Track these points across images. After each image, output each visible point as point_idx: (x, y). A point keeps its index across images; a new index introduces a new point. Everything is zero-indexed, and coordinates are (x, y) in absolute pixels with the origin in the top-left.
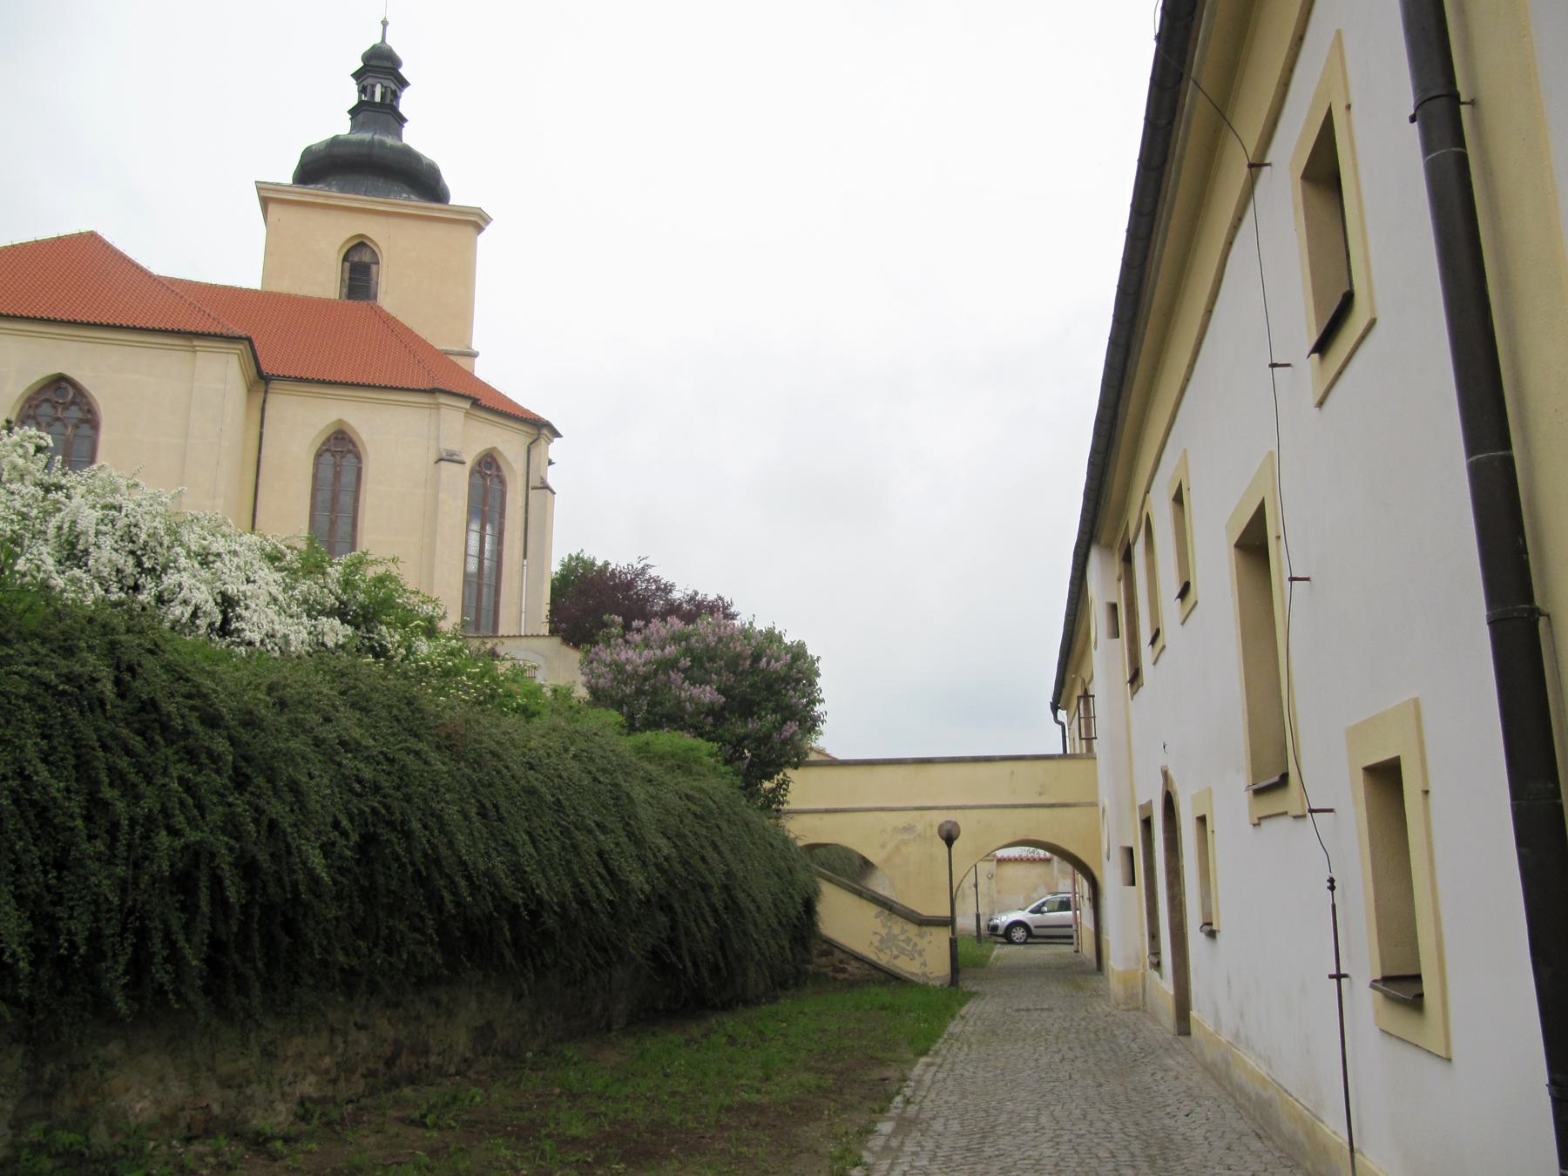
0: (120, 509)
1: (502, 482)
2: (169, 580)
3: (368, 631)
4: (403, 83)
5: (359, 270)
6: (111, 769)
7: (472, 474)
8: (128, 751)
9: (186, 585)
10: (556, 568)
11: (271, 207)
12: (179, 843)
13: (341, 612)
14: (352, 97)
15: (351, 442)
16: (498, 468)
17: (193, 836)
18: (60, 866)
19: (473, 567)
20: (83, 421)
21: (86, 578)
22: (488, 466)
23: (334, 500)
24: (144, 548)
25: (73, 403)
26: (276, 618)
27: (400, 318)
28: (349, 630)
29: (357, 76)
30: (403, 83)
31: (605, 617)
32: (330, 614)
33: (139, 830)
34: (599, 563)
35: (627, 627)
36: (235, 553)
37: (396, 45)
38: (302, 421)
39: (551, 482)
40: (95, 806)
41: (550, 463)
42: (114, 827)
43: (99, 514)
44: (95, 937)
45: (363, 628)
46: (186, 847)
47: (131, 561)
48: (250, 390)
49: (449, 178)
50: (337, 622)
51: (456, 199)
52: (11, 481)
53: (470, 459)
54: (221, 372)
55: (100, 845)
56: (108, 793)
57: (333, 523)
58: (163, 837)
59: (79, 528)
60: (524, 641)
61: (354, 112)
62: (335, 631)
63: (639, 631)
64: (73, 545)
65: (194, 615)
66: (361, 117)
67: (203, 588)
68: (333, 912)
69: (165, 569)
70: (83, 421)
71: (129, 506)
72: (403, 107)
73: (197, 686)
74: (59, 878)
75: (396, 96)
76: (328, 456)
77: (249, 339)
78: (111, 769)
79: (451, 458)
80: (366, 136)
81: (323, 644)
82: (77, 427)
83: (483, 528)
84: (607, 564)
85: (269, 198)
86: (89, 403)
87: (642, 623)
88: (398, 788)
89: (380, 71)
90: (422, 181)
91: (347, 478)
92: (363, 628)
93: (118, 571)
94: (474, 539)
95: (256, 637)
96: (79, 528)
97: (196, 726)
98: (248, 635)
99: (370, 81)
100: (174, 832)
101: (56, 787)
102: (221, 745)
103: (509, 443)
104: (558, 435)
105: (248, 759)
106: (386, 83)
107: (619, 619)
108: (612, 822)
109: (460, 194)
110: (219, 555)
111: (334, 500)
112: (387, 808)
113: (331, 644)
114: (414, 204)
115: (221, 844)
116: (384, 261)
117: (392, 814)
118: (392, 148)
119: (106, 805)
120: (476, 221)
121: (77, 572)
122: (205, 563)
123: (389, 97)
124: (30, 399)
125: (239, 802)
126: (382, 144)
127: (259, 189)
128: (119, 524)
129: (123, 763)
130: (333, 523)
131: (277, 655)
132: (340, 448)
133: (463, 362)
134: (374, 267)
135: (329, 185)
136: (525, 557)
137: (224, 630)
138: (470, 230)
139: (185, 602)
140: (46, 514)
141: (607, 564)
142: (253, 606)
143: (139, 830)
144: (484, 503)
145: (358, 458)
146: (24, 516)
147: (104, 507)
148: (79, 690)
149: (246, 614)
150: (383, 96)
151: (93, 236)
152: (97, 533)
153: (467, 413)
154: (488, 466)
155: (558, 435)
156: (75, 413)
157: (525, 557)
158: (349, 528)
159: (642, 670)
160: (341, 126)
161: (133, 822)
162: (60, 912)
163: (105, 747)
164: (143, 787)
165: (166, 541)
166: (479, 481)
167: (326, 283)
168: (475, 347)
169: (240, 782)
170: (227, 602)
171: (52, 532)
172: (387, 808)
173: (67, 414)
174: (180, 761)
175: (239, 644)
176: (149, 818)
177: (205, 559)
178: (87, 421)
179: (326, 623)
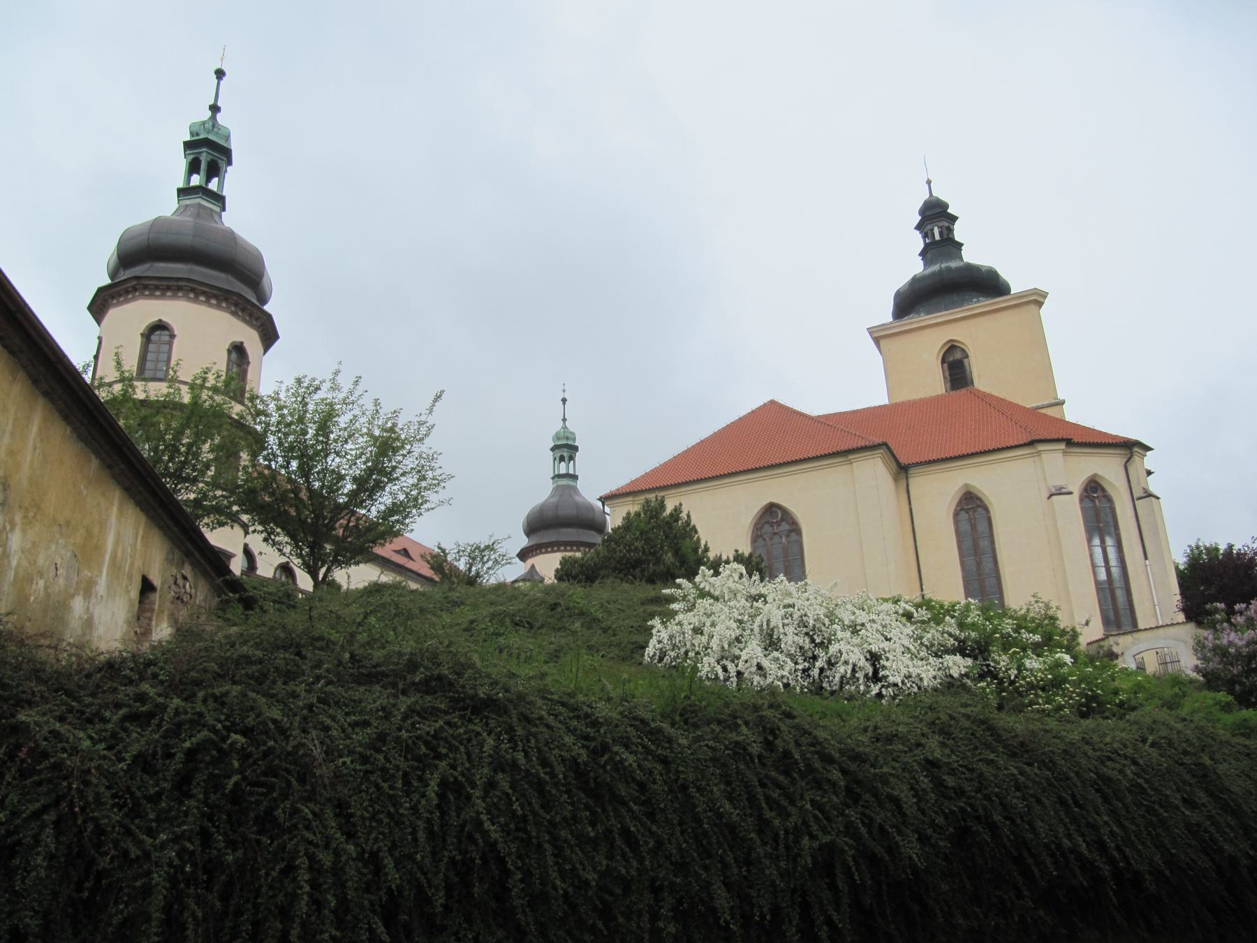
0: (793, 606)
1: (1109, 500)
2: (833, 649)
3: (985, 660)
4: (953, 219)
5: (956, 368)
6: (767, 798)
7: (1081, 500)
8: (778, 785)
9: (844, 651)
10: (1182, 561)
11: (882, 343)
12: (816, 844)
13: (961, 649)
14: (918, 242)
15: (979, 499)
16: (1103, 490)
17: (827, 839)
18: (748, 862)
19: (1103, 576)
20: (791, 531)
21: (782, 657)
22: (1094, 490)
23: (976, 545)
24: (813, 630)
25: (782, 520)
26: (910, 663)
27: (995, 393)
28: (969, 662)
29: (918, 227)
30: (953, 219)
31: (1208, 606)
32: (952, 651)
33: (791, 837)
34: (1222, 547)
35: (1230, 612)
36: (873, 621)
37: (940, 194)
38: (938, 492)
39: (1153, 489)
40: (763, 826)
41: (1149, 473)
42: (776, 838)
43: (783, 612)
44: (776, 910)
45: (980, 658)
46: (821, 847)
47: (807, 640)
48: (896, 480)
49: (1005, 274)
50: (958, 658)
51: (1014, 290)
52: (730, 600)
53: (1077, 489)
54: (872, 472)
55: (768, 848)
56: (768, 814)
57: (979, 564)
58: (806, 841)
59: (772, 625)
60: (1161, 630)
61: (923, 254)
62: (958, 665)
63: (1241, 613)
64: (771, 636)
65: (854, 671)
66: (929, 256)
67: (856, 650)
68: (945, 887)
69: (830, 642)
70: (791, 531)
71: (799, 603)
72: (958, 236)
73: (815, 737)
74: (748, 871)
75: (950, 230)
76: (963, 515)
77: (885, 444)
78: (767, 798)
79: (1060, 492)
80: (935, 268)
81: (951, 676)
82: (788, 536)
83: (1103, 542)
84: (1231, 547)
85: (879, 336)
86: (792, 518)
87: (1244, 606)
88: (978, 790)
89: (935, 215)
90: (986, 285)
91: (982, 527)
92: (980, 658)
93: (801, 648)
94: (1098, 551)
95: (898, 680)
96: (772, 625)
97: (817, 765)
98: (891, 679)
99: (929, 227)
100: (813, 837)
101: (735, 815)
102: (836, 775)
103: (1108, 467)
104: (1149, 449)
105: (858, 782)
106: (941, 224)
107: (1221, 606)
108: (1201, 797)
109: (1017, 286)
110: (863, 625)
111: (976, 545)
112: (972, 806)
113: (956, 675)
114: (983, 304)
115: (845, 842)
116: (971, 352)
117: (976, 811)
118: (958, 269)
119: (768, 822)
120: (1036, 299)
121: (776, 654)
122: (855, 632)
123: (945, 232)
124: (756, 524)
125: (853, 814)
126: (949, 269)
127: (871, 334)
128: (795, 616)
129: (775, 794)
130: (979, 564)
131: (916, 690)
132: (971, 507)
133: (1049, 412)
134: (966, 361)
135: (918, 313)
136: (1146, 558)
137: (876, 678)
138: (1033, 307)
139: (846, 663)
140: (753, 617)
141: (1231, 547)
142: (891, 657)
143: (791, 837)
144: (1098, 521)
145: (987, 510)
146: (740, 622)
147: (785, 607)
148: (740, 750)
149: (887, 664)
150: (941, 234)
151: (772, 402)
152: (784, 625)
153: (1065, 453)
154: (1094, 490)
155: (1149, 449)
156: (785, 527)
157: (1146, 558)
158: (992, 566)
159: (1245, 651)
160: (916, 267)
161: (787, 832)
162: (753, 893)
163: (763, 785)
164: (790, 808)
165: (827, 621)
166: (1088, 504)
167: (934, 383)
168: (1060, 397)
169: (853, 796)
170: (874, 658)
171: (757, 630)
172: (972, 806)
173: (781, 528)
174: (812, 788)
175: (887, 687)
176: (796, 827)
177: (855, 629)
178: (793, 531)
179: (949, 659)
